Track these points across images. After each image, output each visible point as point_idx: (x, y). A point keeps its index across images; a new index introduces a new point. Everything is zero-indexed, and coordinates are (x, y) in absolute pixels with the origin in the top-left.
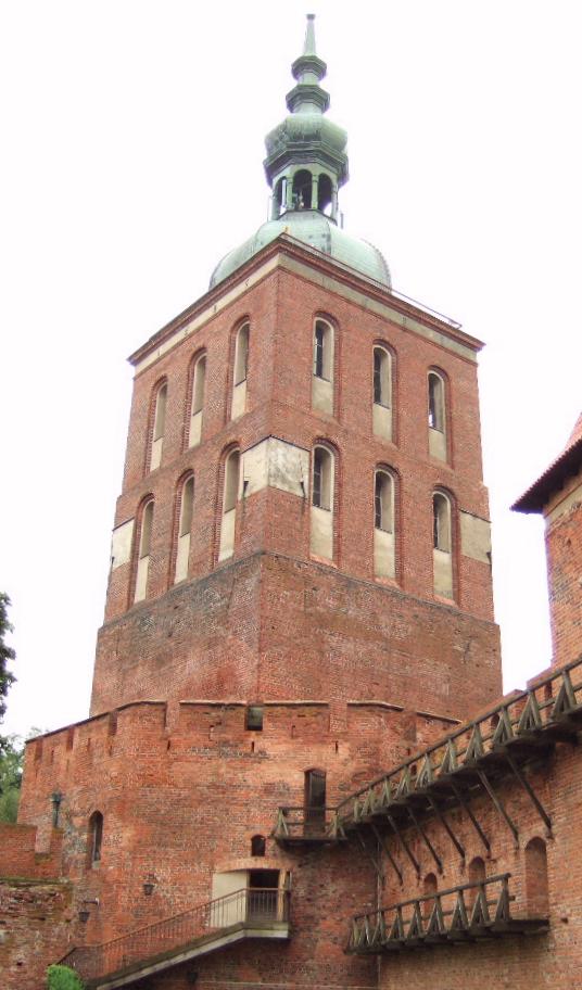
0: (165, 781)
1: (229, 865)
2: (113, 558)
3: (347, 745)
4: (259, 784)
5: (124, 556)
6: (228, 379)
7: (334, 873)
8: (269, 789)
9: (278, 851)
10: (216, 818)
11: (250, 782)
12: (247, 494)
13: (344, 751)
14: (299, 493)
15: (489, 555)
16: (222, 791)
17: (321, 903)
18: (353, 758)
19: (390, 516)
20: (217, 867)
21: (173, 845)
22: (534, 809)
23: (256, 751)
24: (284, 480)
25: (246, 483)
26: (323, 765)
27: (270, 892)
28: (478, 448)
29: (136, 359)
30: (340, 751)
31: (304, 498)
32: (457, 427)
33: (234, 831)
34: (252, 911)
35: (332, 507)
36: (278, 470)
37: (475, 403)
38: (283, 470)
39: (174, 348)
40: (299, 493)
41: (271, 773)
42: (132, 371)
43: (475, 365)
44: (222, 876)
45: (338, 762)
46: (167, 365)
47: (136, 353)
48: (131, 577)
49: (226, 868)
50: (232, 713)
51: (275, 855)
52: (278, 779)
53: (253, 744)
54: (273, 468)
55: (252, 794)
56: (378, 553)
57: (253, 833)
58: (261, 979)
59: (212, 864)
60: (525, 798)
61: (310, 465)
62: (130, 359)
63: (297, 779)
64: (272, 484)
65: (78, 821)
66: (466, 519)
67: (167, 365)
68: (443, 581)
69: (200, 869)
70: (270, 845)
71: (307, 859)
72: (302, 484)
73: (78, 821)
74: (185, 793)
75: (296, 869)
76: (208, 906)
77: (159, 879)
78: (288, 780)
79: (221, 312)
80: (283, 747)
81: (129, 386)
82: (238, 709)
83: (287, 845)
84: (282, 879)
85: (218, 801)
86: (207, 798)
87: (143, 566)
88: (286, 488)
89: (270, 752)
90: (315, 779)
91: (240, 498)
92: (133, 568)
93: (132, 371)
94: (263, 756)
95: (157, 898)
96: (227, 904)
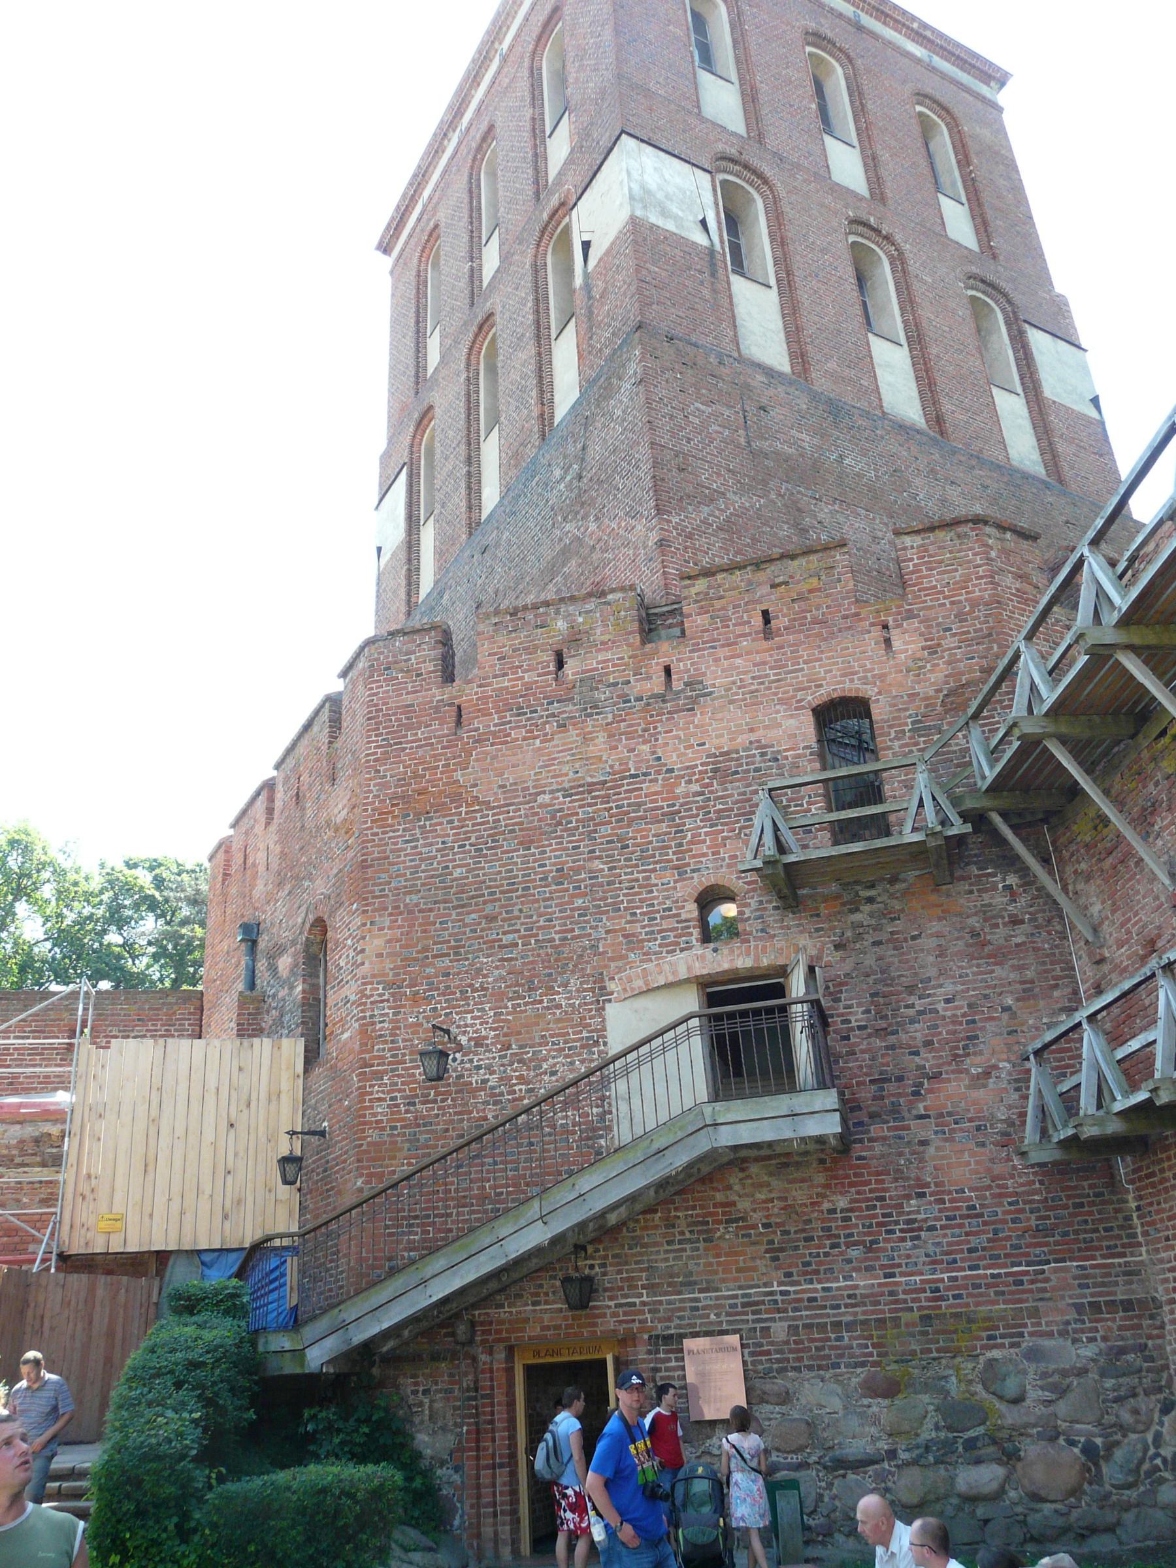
2: (379, 549)
4: (696, 758)
5: (396, 533)
6: (536, 125)
8: (722, 768)
10: (597, 864)
12: (592, 263)
13: (906, 643)
14: (700, 238)
15: (1095, 401)
17: (918, 1032)
18: (933, 650)
19: (894, 318)
23: (677, 685)
24: (664, 213)
25: (586, 245)
26: (857, 684)
27: (770, 1011)
29: (385, 248)
30: (897, 644)
31: (711, 251)
32: (986, 196)
33: (649, 888)
34: (726, 1075)
35: (773, 281)
36: (648, 192)
37: (1011, 166)
38: (660, 195)
40: (700, 238)
41: (719, 729)
42: (387, 262)
43: (1000, 110)
45: (893, 670)
47: (389, 226)
48: (409, 560)
49: (639, 984)
52: (743, 739)
53: (668, 670)
54: (636, 187)
56: (885, 378)
61: (715, 195)
62: (379, 247)
64: (638, 213)
65: (284, 963)
66: (1038, 340)
67: (435, 209)
68: (1022, 446)
72: (703, 223)
73: (284, 963)
75: (831, 956)
76: (601, 1073)
77: (464, 1040)
81: (387, 282)
83: (789, 884)
84: (797, 986)
87: (428, 537)
88: (670, 226)
90: (842, 721)
91: (578, 281)
92: (411, 546)
93: (387, 262)
95: (465, 1088)
96: (666, 1092)
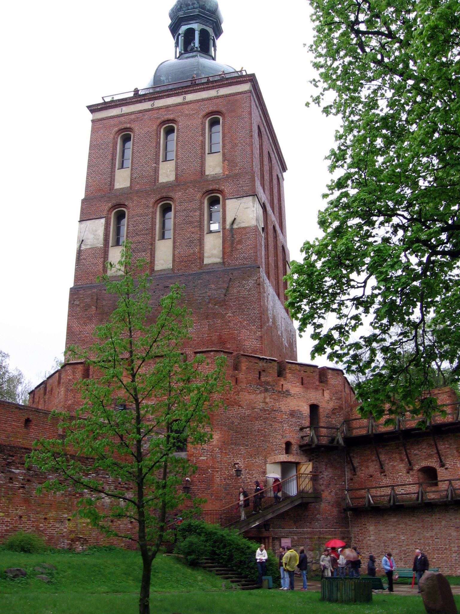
0: (236, 403)
1: (274, 459)
3: (328, 391)
7: (326, 465)
8: (292, 414)
9: (299, 451)
10: (266, 430)
11: (283, 409)
16: (268, 415)
20: (268, 460)
21: (243, 445)
22: (434, 446)
28: (90, 166)
29: (93, 109)
30: (325, 395)
39: (140, 112)
42: (90, 116)
44: (272, 465)
46: (134, 121)
49: (273, 461)
50: (271, 365)
51: (297, 453)
53: (282, 385)
55: (284, 416)
57: (285, 440)
58: (295, 527)
59: (265, 458)
60: (432, 442)
63: (306, 410)
67: (134, 121)
69: (259, 460)
70: (295, 448)
71: (313, 457)
74: (248, 412)
78: (302, 409)
79: (188, 103)
80: (297, 389)
81: (89, 126)
82: (274, 363)
85: (267, 418)
86: (261, 417)
89: (292, 392)
90: (314, 408)
94: (287, 394)
